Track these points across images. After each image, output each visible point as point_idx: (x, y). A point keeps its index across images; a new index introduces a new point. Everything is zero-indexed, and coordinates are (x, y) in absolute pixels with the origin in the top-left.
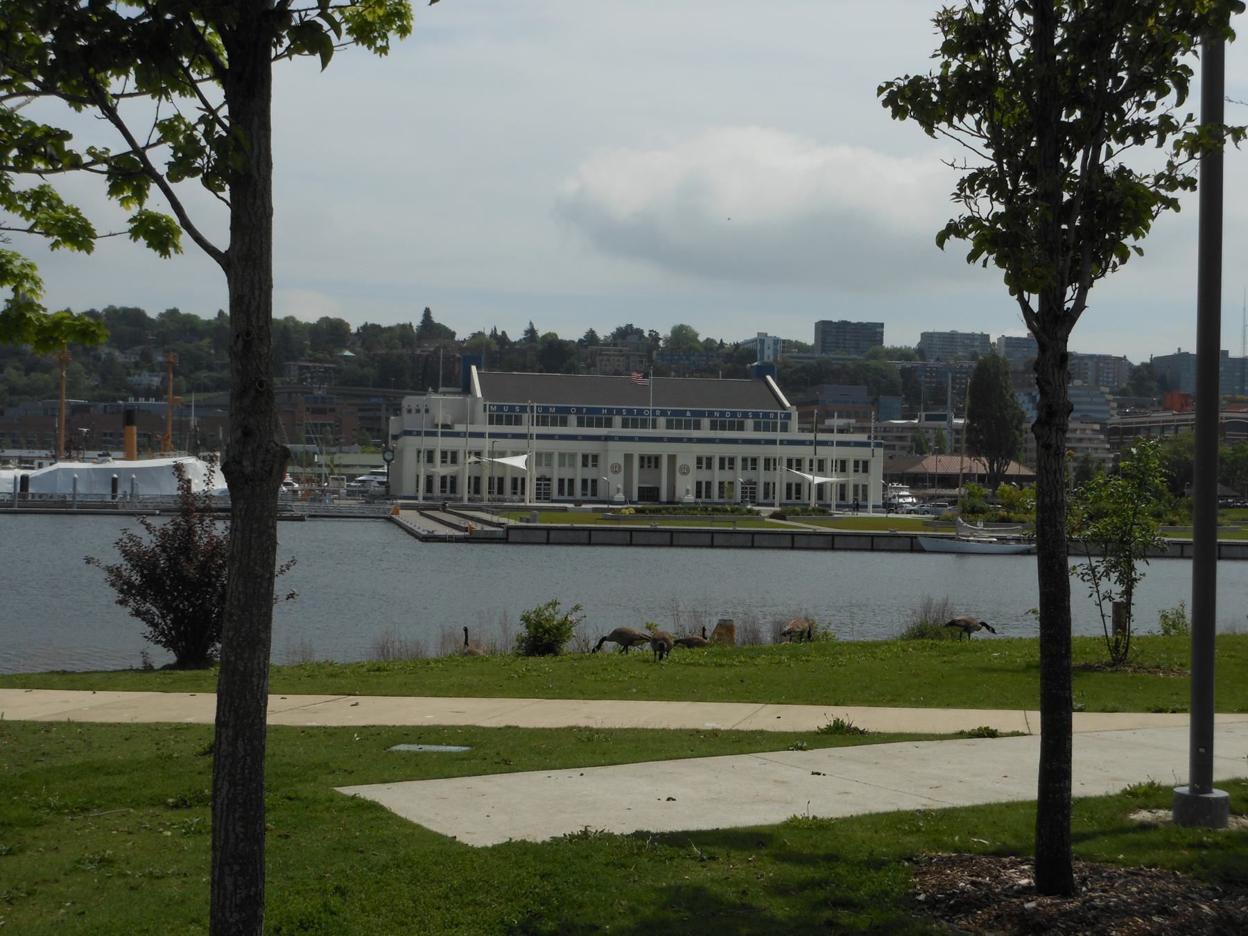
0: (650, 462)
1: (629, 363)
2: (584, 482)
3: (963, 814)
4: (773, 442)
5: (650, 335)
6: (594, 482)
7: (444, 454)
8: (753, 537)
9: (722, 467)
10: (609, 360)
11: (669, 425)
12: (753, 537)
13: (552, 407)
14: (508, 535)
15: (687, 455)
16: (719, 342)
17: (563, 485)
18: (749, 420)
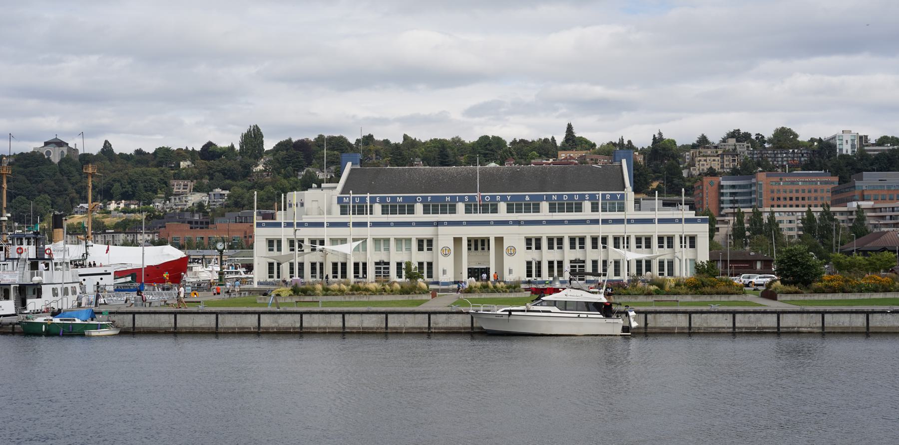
1: (723, 162)
2: (551, 264)
5: (757, 138)
6: (430, 265)
7: (661, 239)
8: (301, 318)
9: (551, 247)
10: (705, 161)
11: (510, 210)
12: (301, 318)
13: (400, 197)
15: (515, 237)
16: (414, 139)
17: (641, 266)
18: (376, 204)
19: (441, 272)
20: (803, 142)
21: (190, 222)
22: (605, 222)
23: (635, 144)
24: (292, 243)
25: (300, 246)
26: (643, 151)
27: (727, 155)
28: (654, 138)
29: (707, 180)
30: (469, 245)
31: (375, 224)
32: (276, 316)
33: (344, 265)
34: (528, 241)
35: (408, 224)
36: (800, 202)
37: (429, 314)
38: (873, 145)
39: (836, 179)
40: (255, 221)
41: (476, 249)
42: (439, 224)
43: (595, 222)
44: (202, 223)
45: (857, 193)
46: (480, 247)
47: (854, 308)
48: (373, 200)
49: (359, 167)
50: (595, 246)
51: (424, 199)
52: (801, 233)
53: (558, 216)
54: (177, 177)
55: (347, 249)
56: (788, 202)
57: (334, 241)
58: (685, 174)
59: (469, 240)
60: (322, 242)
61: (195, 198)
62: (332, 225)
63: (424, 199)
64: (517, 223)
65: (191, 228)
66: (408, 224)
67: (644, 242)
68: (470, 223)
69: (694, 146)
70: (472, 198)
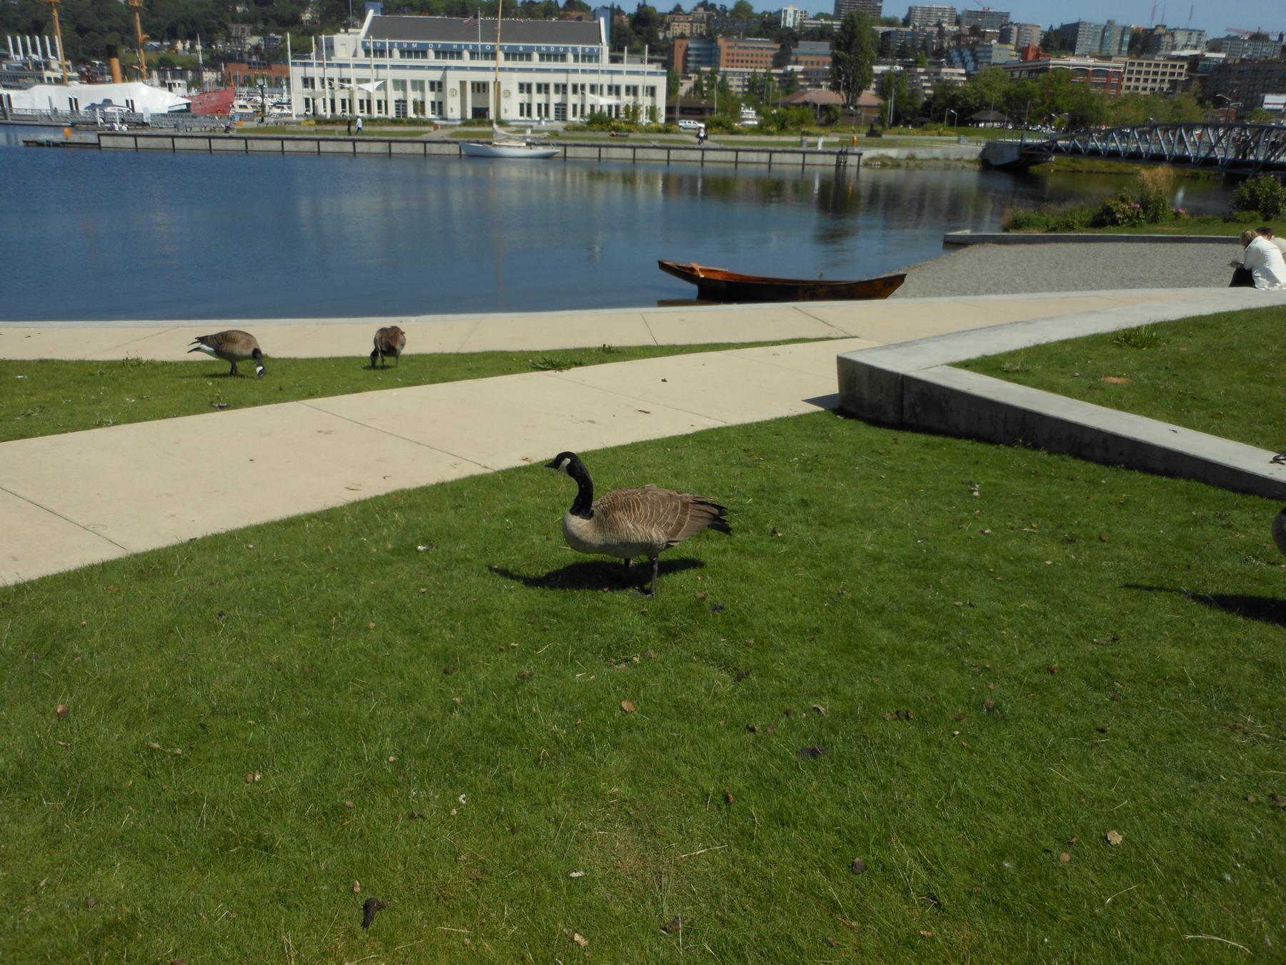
0: (480, 88)
2: (539, 106)
3: (726, 431)
4: (620, 72)
14: (99, 140)
15: (510, 82)
19: (449, 110)
20: (756, 14)
21: (249, 63)
22: (584, 71)
23: (623, 8)
24: (322, 81)
25: (330, 84)
26: (629, 15)
27: (696, 22)
28: (639, 5)
29: (678, 42)
30: (473, 88)
31: (394, 67)
32: (296, 142)
33: (369, 102)
34: (521, 86)
35: (421, 68)
36: (749, 64)
37: (425, 142)
38: (810, 19)
39: (778, 46)
40: (290, 61)
41: (479, 91)
42: (447, 68)
43: (576, 71)
44: (259, 64)
45: (793, 58)
46: (481, 90)
47: (761, 148)
48: (392, 45)
49: (380, 15)
50: (539, 91)
51: (400, 45)
52: (746, 90)
53: (546, 65)
54: (234, 20)
55: (370, 87)
56: (740, 64)
57: (360, 81)
58: (661, 36)
59: (473, 84)
60: (349, 81)
61: (254, 40)
62: (357, 66)
63: (400, 45)
64: (512, 70)
65: (250, 68)
66: (421, 68)
67: (613, 90)
68: (473, 69)
69: (671, 13)
70: (476, 47)
